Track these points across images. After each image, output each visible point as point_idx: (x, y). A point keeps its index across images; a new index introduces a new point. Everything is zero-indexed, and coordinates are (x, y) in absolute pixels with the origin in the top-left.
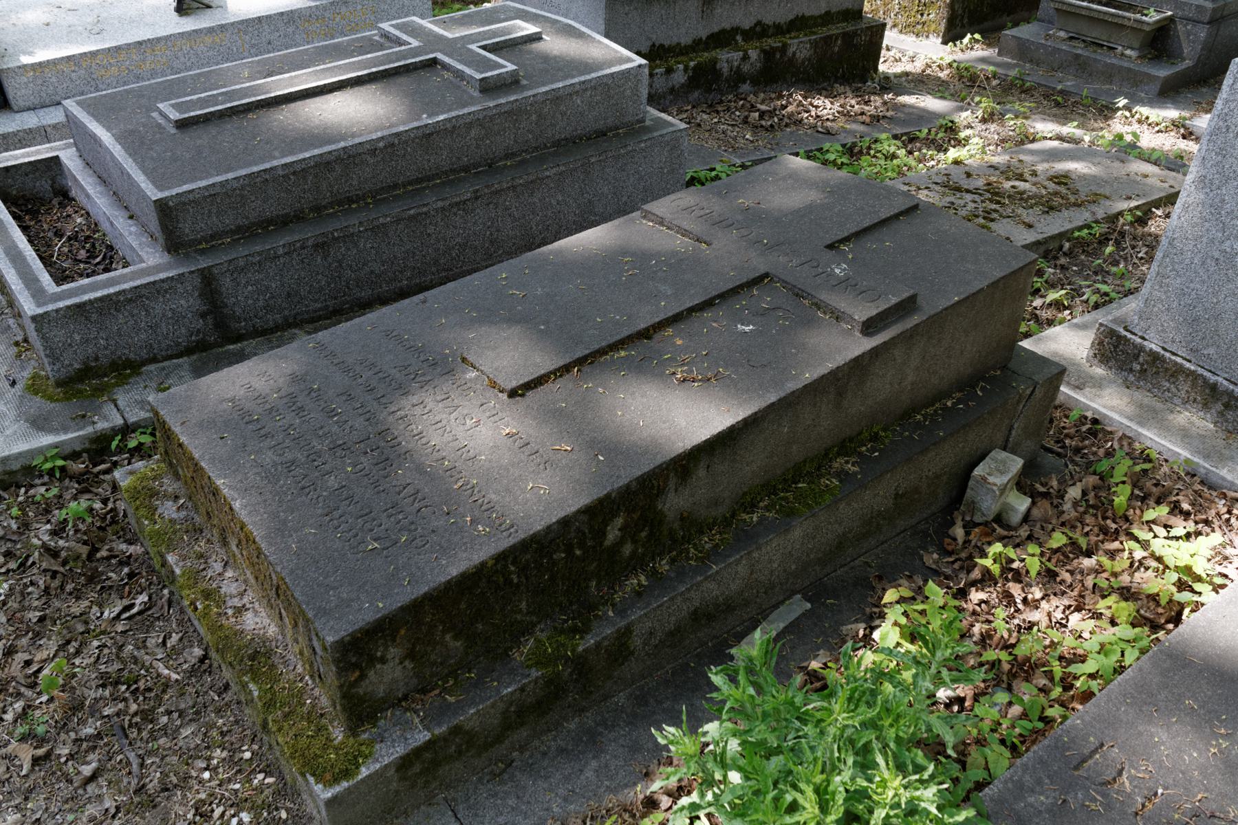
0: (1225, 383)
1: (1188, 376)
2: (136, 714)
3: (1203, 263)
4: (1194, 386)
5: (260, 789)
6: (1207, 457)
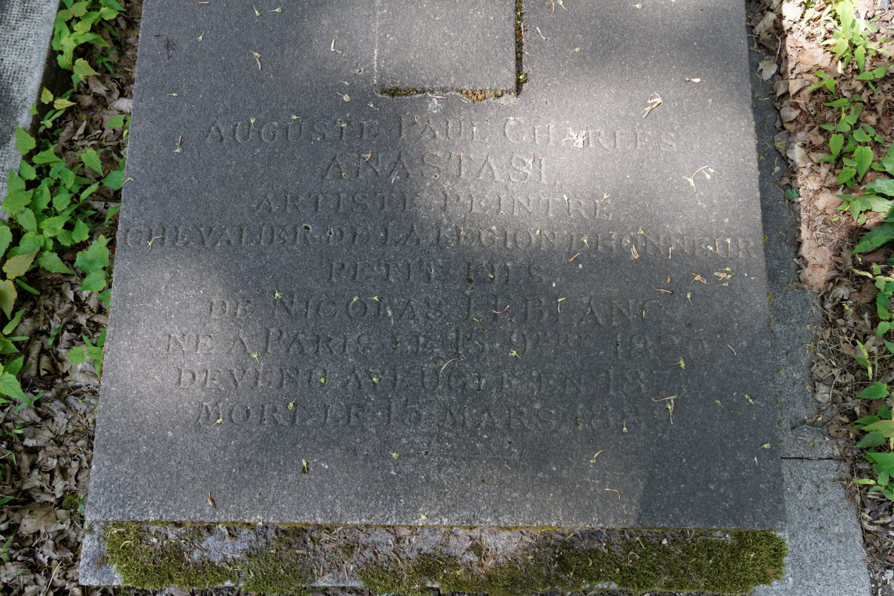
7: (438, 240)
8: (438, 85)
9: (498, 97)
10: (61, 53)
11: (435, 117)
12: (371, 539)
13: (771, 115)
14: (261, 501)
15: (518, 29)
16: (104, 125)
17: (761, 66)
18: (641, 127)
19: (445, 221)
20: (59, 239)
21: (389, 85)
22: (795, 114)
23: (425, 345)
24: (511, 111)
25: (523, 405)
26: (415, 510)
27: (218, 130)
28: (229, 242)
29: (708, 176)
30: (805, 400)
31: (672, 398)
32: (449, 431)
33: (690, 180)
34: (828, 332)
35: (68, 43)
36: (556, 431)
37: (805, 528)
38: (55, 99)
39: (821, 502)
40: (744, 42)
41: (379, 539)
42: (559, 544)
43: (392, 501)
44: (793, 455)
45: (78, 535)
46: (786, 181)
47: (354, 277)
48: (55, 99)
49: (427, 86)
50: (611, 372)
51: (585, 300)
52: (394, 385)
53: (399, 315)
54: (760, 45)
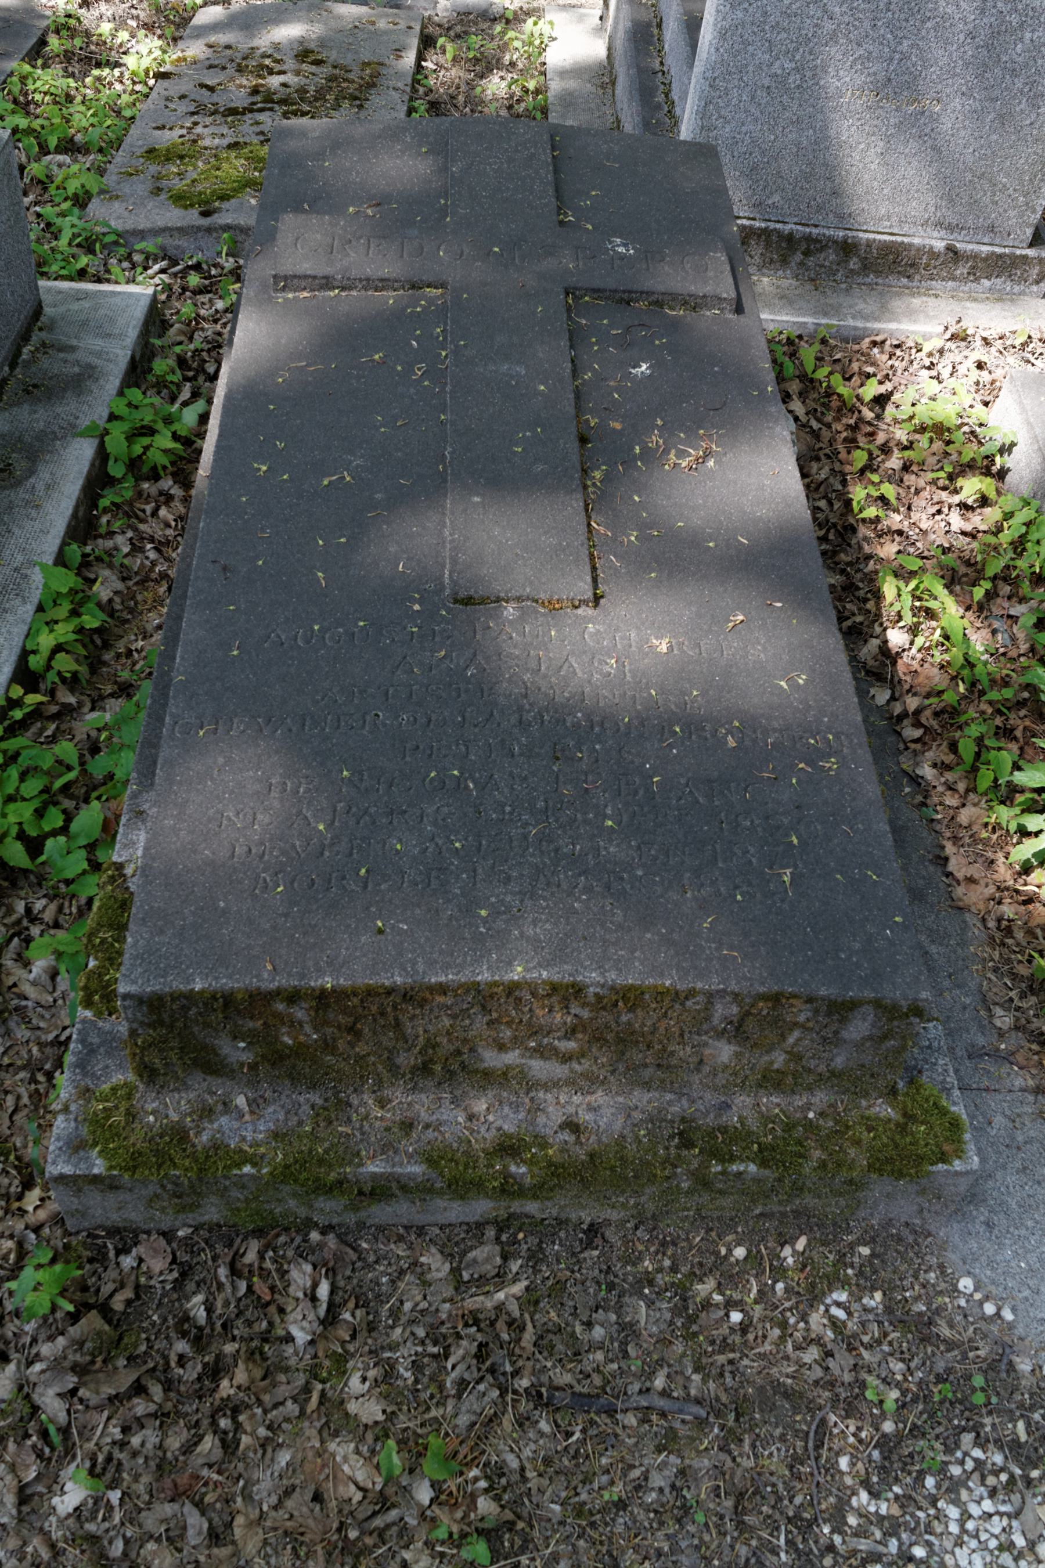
0: (799, 228)
1: (759, 236)
2: (902, 1406)
3: (753, 98)
4: (768, 244)
5: (804, 1262)
6: (826, 314)
7: (520, 722)
8: (513, 593)
9: (577, 607)
10: (34, 652)
11: (511, 622)
12: (434, 1117)
13: (892, 739)
14: (329, 964)
15: (591, 555)
16: (76, 732)
17: (872, 691)
18: (725, 639)
19: (527, 707)
20: (26, 827)
21: (463, 594)
22: (918, 733)
23: (511, 813)
24: (588, 620)
25: (624, 871)
26: (510, 964)
27: (278, 636)
28: (290, 730)
29: (801, 681)
30: (981, 1027)
31: (788, 871)
32: (543, 890)
33: (783, 683)
34: (997, 953)
35: (46, 641)
36: (662, 896)
37: (1004, 1167)
38: (25, 694)
39: (1020, 1138)
40: (848, 676)
41: (445, 1117)
42: (677, 1119)
43: (482, 956)
44: (974, 1086)
45: (10, 1184)
46: (919, 798)
47: (430, 756)
48: (25, 694)
49: (502, 595)
50: (718, 847)
51: (683, 781)
52: (479, 851)
53: (481, 787)
54: (868, 673)
